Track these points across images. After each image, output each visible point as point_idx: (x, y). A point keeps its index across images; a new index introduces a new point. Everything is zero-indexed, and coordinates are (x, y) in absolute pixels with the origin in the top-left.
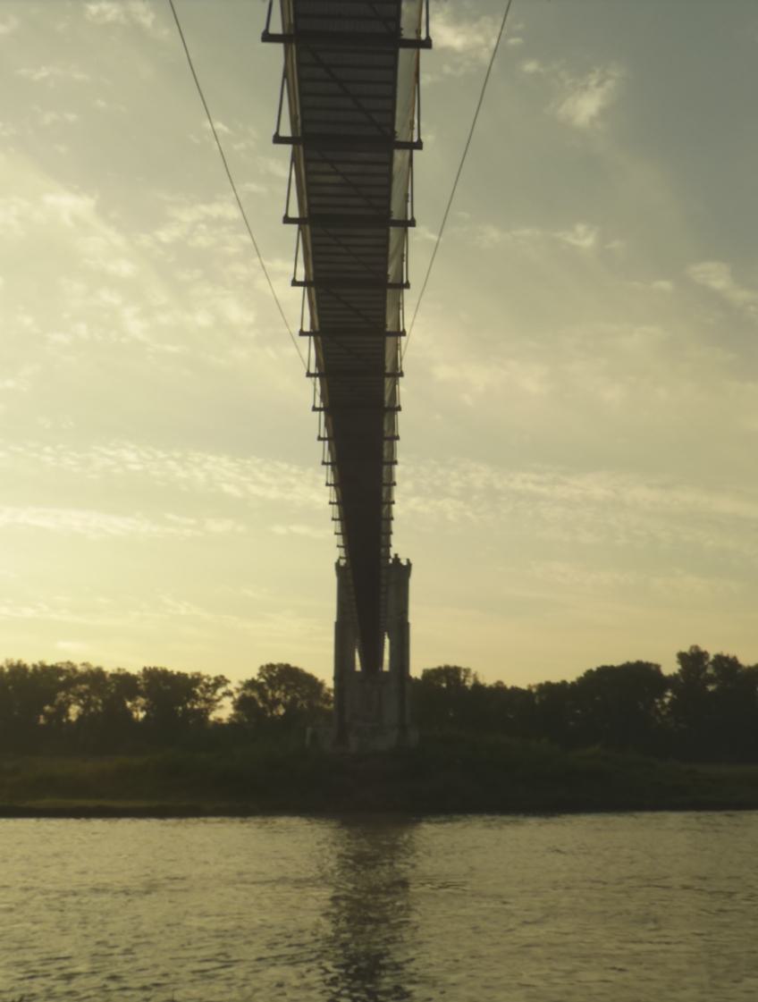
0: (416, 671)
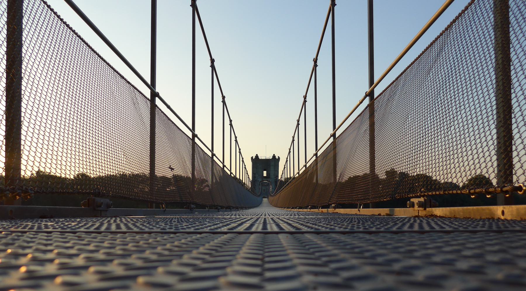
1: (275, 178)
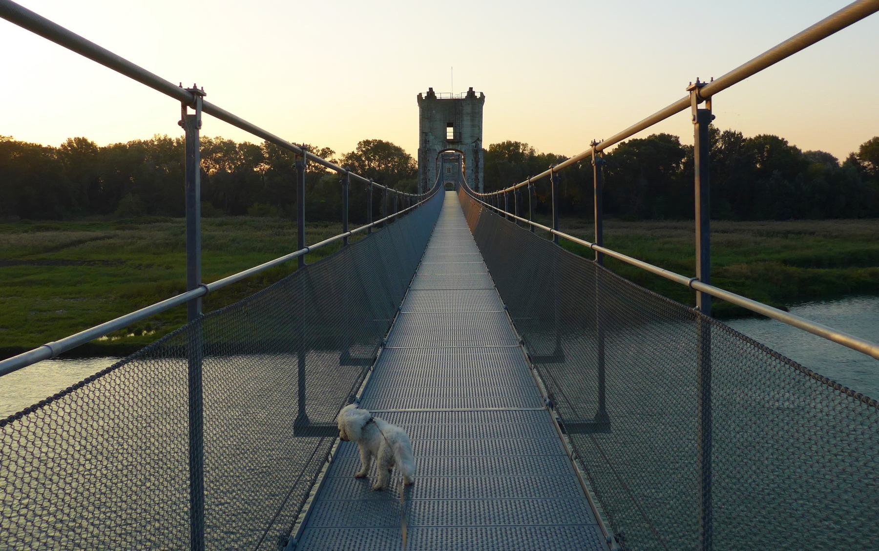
0: (486, 145)
1: (474, 144)
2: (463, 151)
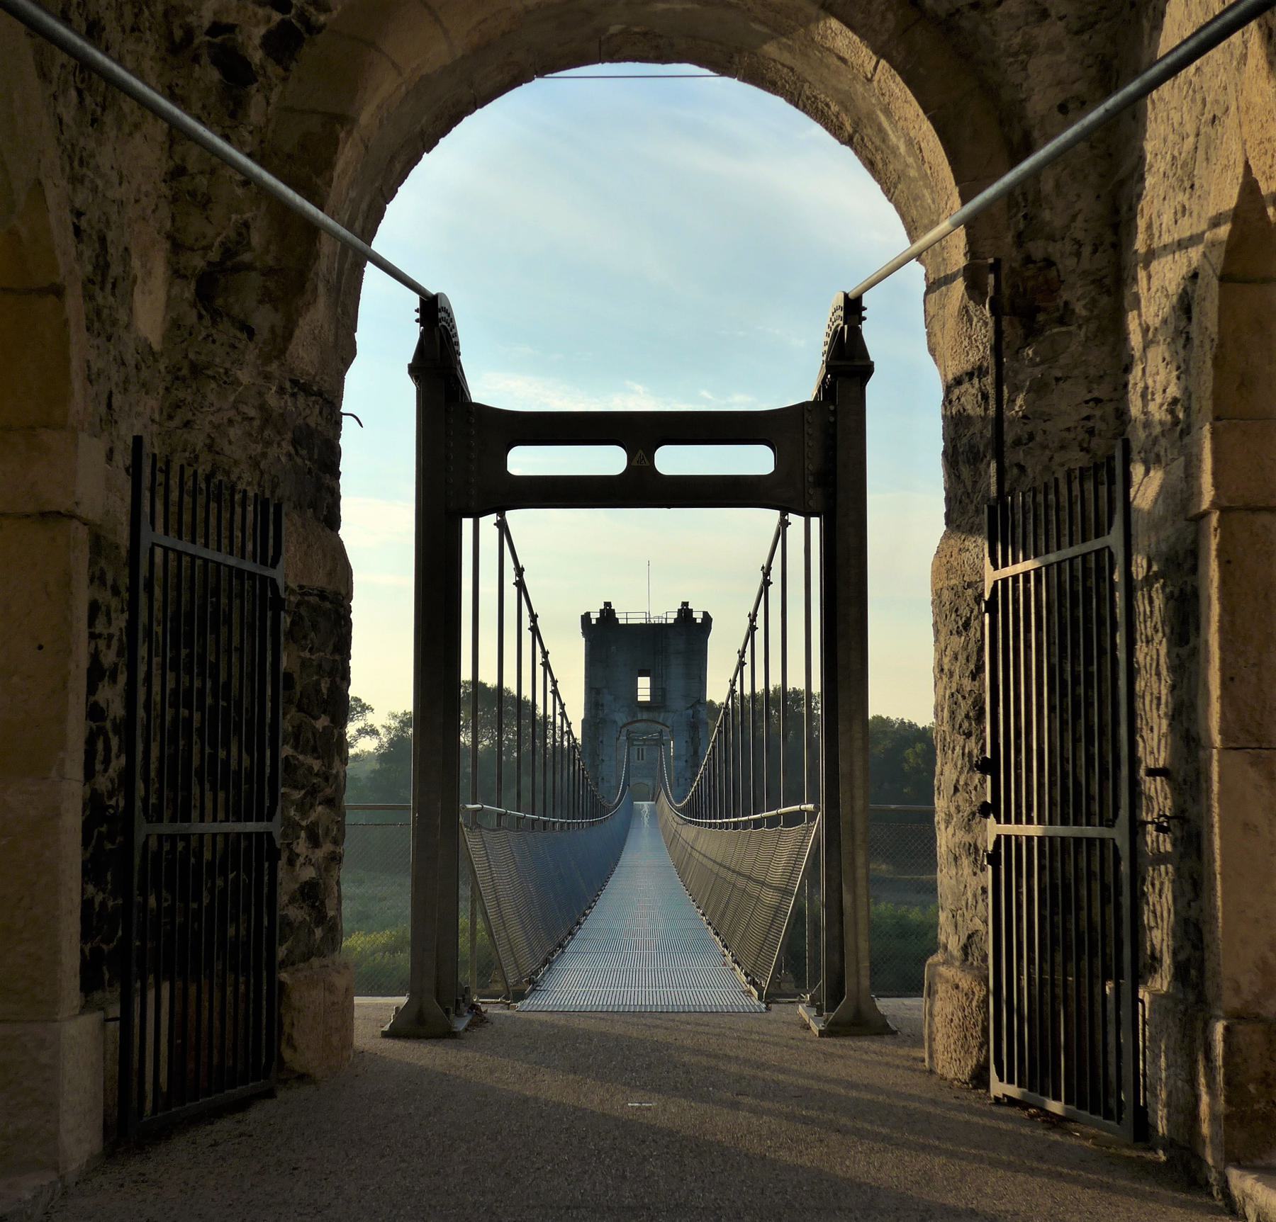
0: (368, 263)
1: (690, 712)
2: (668, 725)
